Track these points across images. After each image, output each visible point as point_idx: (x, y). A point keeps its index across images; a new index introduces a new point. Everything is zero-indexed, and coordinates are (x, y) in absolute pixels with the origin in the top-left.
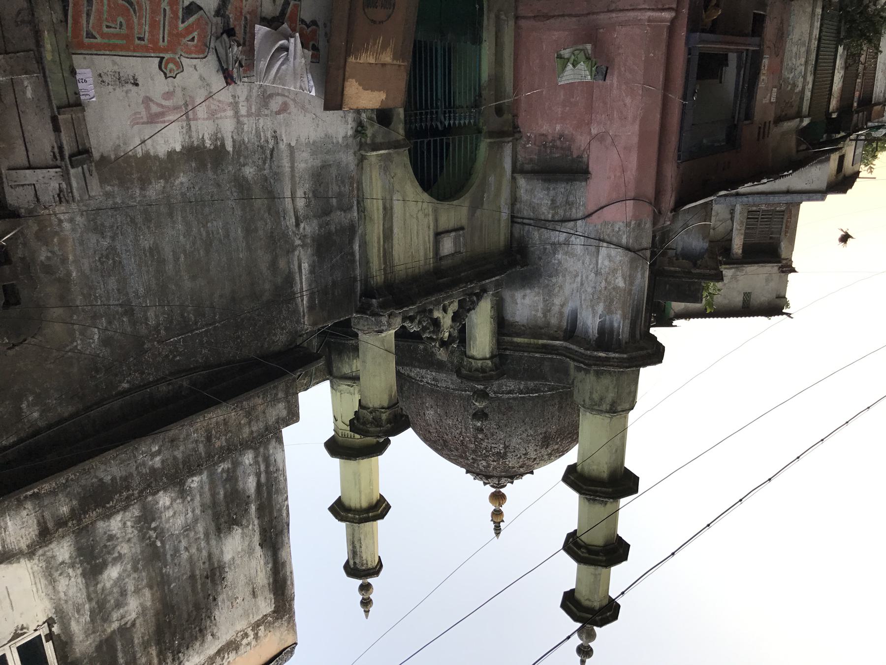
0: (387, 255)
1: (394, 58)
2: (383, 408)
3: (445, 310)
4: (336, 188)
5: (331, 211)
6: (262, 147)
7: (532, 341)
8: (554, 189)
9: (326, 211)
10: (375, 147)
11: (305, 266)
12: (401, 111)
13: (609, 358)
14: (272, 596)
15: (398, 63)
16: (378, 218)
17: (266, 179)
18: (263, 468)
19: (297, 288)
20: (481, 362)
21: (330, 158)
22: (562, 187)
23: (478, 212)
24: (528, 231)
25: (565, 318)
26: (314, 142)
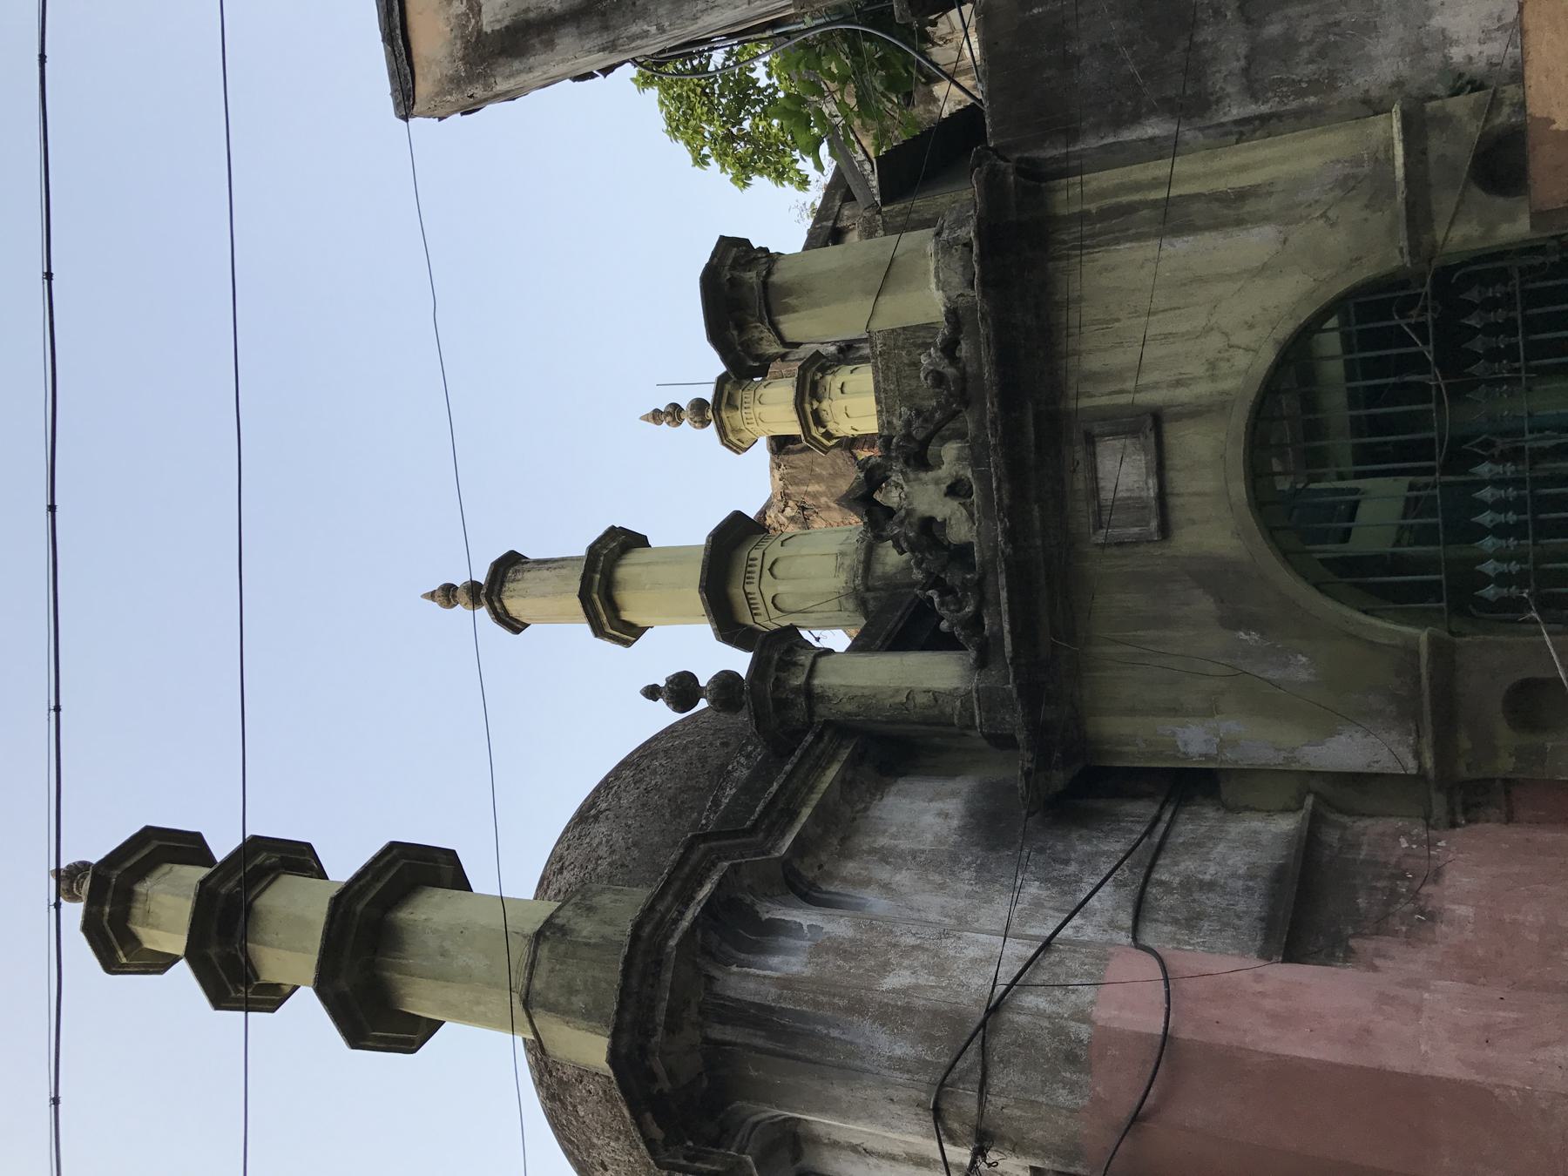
0: (1119, 221)
2: (769, 273)
3: (956, 490)
4: (1305, 32)
5: (1248, 21)
7: (816, 798)
8: (1248, 889)
10: (1414, 128)
12: (1517, 227)
13: (687, 906)
14: (506, 23)
22: (1252, 906)
23: (1205, 604)
24: (1131, 831)
25: (850, 890)
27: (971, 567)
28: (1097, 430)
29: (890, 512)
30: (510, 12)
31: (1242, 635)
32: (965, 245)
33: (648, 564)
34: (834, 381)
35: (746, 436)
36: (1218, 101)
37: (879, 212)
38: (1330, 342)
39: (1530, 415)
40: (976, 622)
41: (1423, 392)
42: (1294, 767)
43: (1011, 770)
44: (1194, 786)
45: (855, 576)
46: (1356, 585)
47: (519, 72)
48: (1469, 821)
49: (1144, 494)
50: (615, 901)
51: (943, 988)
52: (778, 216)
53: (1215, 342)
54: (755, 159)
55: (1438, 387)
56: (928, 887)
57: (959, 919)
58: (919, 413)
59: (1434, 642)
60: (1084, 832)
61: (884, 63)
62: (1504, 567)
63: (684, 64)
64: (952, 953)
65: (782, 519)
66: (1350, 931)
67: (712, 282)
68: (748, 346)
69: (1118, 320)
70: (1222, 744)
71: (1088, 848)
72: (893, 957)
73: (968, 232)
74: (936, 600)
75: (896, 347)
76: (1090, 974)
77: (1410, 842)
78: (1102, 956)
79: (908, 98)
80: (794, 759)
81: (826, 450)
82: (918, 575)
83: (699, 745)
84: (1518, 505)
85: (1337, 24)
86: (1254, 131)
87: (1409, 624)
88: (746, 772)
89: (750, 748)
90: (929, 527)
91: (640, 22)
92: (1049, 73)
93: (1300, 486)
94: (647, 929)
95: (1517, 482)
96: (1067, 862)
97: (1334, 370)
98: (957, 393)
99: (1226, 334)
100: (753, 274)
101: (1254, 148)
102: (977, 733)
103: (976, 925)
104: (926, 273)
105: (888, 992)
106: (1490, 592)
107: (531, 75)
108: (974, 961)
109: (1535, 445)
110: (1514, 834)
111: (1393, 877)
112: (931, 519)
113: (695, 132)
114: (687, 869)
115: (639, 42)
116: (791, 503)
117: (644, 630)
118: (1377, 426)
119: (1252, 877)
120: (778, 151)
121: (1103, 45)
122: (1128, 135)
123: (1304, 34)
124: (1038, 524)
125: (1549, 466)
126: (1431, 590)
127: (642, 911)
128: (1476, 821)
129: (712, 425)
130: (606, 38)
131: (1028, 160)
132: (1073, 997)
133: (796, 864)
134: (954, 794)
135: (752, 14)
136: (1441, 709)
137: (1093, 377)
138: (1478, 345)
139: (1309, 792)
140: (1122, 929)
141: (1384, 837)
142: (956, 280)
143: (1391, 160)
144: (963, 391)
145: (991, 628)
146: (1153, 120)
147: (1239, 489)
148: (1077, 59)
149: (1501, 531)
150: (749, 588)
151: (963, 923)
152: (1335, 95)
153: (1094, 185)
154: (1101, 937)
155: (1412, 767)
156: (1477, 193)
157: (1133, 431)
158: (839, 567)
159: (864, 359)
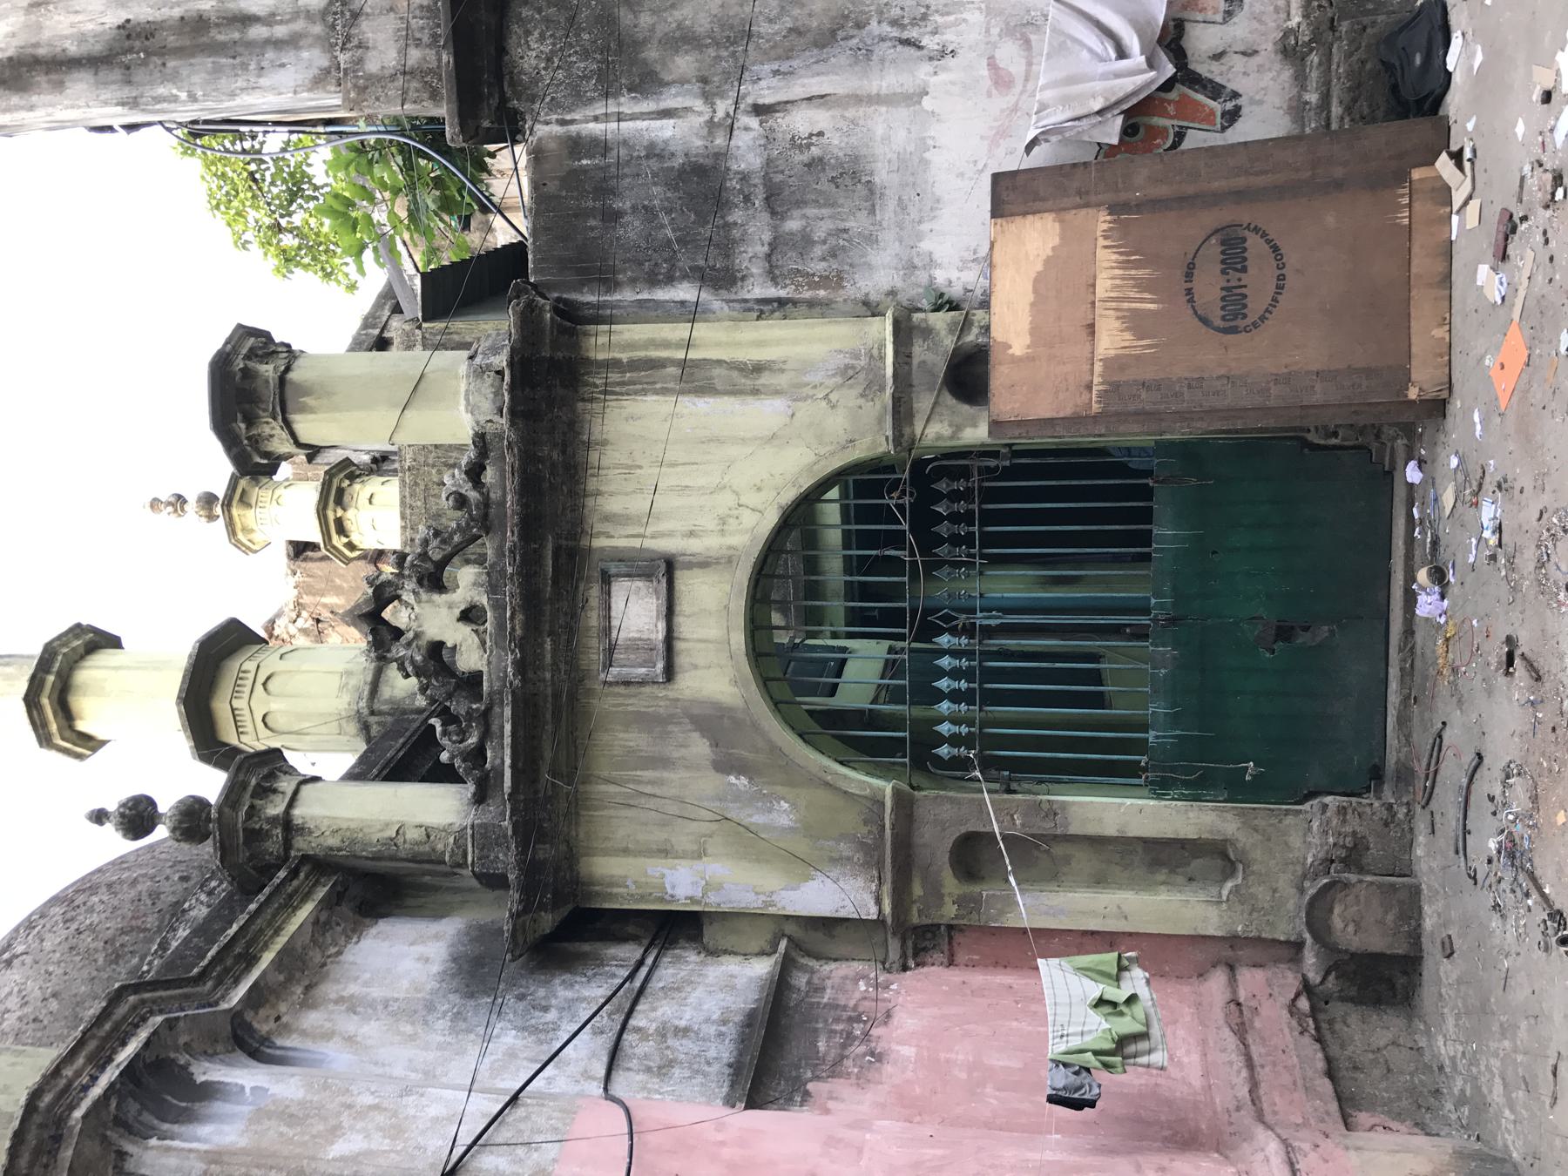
0: (644, 372)
2: (288, 369)
3: (470, 615)
5: (773, 213)
6: (924, 17)
7: (281, 941)
8: (720, 1035)
9: (776, 200)
10: (904, 332)
11: (665, 130)
12: (977, 433)
13: (102, 1069)
15: (1096, 380)
16: (738, 344)
17: (860, 26)
19: (627, 105)
20: (290, 790)
21: (887, 213)
22: (723, 1051)
23: (700, 747)
24: (614, 976)
26: (925, 163)
27: (478, 697)
28: (613, 571)
29: (398, 633)
30: (16, 42)
32: (498, 372)
33: (116, 668)
34: (361, 491)
36: (743, 278)
37: (419, 327)
38: (831, 511)
39: (981, 595)
40: (478, 754)
41: (895, 566)
42: (772, 910)
43: (499, 912)
44: (677, 928)
46: (834, 736)
47: (18, 108)
48: (917, 965)
49: (653, 636)
51: (397, 1152)
52: (319, 316)
53: (726, 500)
54: (306, 254)
55: (914, 564)
57: (426, 1073)
58: (437, 534)
59: (897, 793)
60: (567, 977)
61: (438, 183)
62: (956, 729)
63: (233, 144)
64: (412, 1112)
66: (809, 1074)
68: (255, 441)
69: (640, 467)
70: (708, 887)
71: (569, 994)
72: (345, 1119)
73: (501, 360)
74: (439, 729)
75: (426, 464)
76: (556, 1129)
77: (867, 985)
79: (466, 224)
80: (261, 897)
82: (421, 702)
83: (152, 878)
84: (967, 674)
85: (846, 231)
86: (773, 312)
87: (879, 777)
88: (205, 911)
89: (214, 884)
91: (170, 85)
92: (592, 222)
93: (797, 641)
94: (47, 1098)
96: (546, 1009)
97: (834, 537)
99: (1500, 545)
100: (270, 367)
101: (772, 326)
102: (467, 872)
103: (444, 1080)
104: (457, 393)
106: (944, 751)
107: (31, 114)
110: (954, 976)
112: (441, 644)
113: (239, 214)
114: (108, 1026)
115: (165, 105)
116: (305, 614)
117: (103, 743)
118: (865, 592)
119: (724, 1022)
120: (326, 251)
121: (644, 207)
122: (661, 294)
123: (819, 234)
125: (996, 643)
126: (894, 747)
127: (44, 1076)
129: (221, 522)
130: (127, 92)
131: (566, 302)
132: (535, 1155)
133: (249, 1016)
134: (437, 937)
135: (300, 105)
136: (900, 861)
137: (607, 518)
138: (944, 529)
140: (594, 1079)
141: (843, 979)
142: (487, 406)
143: (882, 358)
146: (685, 285)
147: (739, 639)
149: (955, 697)
150: (236, 704)
151: (430, 1076)
152: (842, 292)
154: (573, 1089)
155: (871, 912)
156: (949, 399)
157: (647, 575)
158: (342, 688)
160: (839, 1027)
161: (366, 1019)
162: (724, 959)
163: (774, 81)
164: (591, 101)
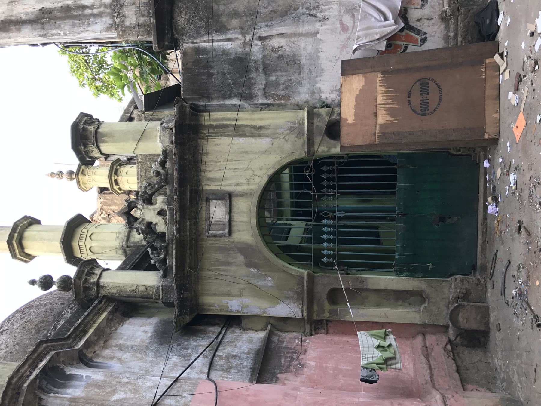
0: (221, 129)
1: (381, 125)
2: (98, 128)
3: (161, 213)
4: (282, 80)
5: (266, 74)
6: (318, 6)
7: (96, 325)
8: (248, 358)
9: (267, 70)
10: (311, 115)
11: (228, 45)
12: (336, 150)
13: (34, 370)
15: (377, 132)
18: (96, 11)
19: (215, 37)
21: (305, 74)
22: (248, 364)
23: (241, 259)
24: (211, 337)
25: (105, 361)
26: (318, 57)
28: (211, 197)
29: (136, 219)
31: (252, 269)
32: (171, 129)
33: (39, 231)
34: (124, 170)
35: (88, 186)
36: (256, 97)
37: (144, 113)
38: (286, 177)
39: (338, 206)
40: (164, 261)
41: (308, 196)
42: (265, 315)
43: (171, 315)
44: (232, 321)
45: (123, 241)
47: (5, 38)
48: (316, 334)
49: (224, 220)
50: (3, 368)
51: (136, 398)
52: (109, 110)
53: (250, 173)
55: (314, 195)
56: (136, 359)
57: (146, 371)
58: (150, 185)
59: (309, 274)
60: (195, 338)
61: (150, 63)
63: (79, 50)
64: (141, 384)
65: (100, 218)
66: (278, 371)
67: (75, 128)
68: (87, 153)
69: (220, 162)
70: (243, 306)
71: (195, 344)
72: (118, 387)
73: (172, 125)
74: (150, 252)
75: (146, 161)
76: (191, 391)
77: (299, 341)
78: (195, 383)
79: (160, 78)
80: (89, 310)
81: (119, 194)
82: (144, 243)
83: (51, 304)
84: (333, 233)
85: (291, 80)
86: (266, 108)
88: (69, 315)
89: (72, 306)
90: (150, 227)
92: (203, 77)
94: (15, 380)
95: (333, 226)
96: (187, 349)
98: (166, 180)
100: (92, 127)
102: (160, 302)
103: (152, 373)
105: (114, 401)
106: (325, 260)
107: (10, 40)
108: (149, 387)
109: (339, 215)
110: (328, 338)
111: (292, 353)
112: (151, 223)
114: (36, 355)
115: (56, 37)
116: (104, 212)
117: (34, 257)
119: (249, 353)
120: (111, 87)
121: (221, 72)
122: (227, 102)
124: (188, 228)
125: (342, 223)
126: (308, 258)
127: (14, 372)
128: (318, 333)
129: (75, 181)
130: (42, 32)
131: (194, 105)
132: (184, 399)
136: (309, 298)
137: (209, 179)
138: (325, 183)
139: (269, 323)
140: (204, 373)
141: (290, 339)
142: (167, 141)
143: (303, 124)
144: (166, 179)
145: (169, 264)
146: (236, 99)
147: (254, 221)
148: (212, 75)
149: (329, 241)
150: (80, 243)
151: (147, 372)
152: (289, 101)
153: (215, 116)
154: (197, 376)
157: (222, 199)
158: (117, 238)
159: (135, 163)
160: (288, 355)
161: (125, 352)
162: (249, 332)
163: (266, 29)
164: (203, 35)
